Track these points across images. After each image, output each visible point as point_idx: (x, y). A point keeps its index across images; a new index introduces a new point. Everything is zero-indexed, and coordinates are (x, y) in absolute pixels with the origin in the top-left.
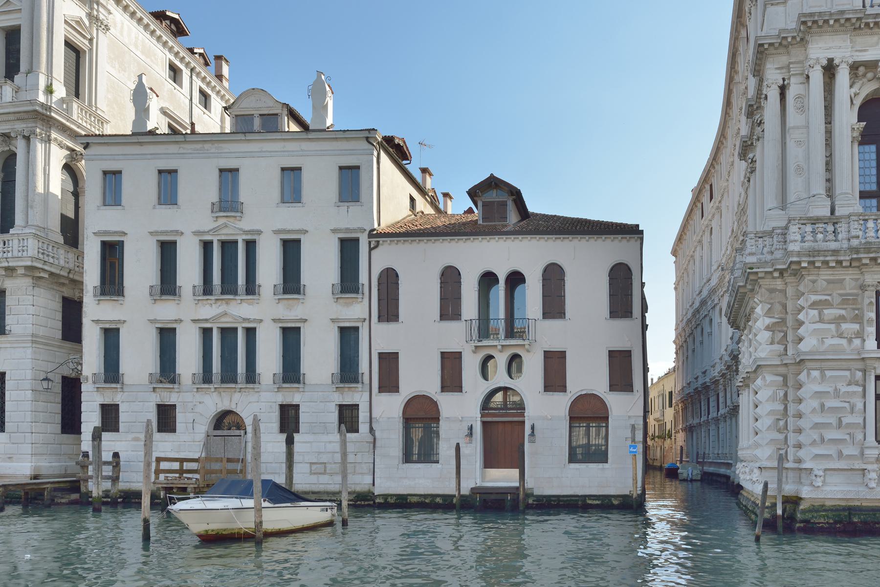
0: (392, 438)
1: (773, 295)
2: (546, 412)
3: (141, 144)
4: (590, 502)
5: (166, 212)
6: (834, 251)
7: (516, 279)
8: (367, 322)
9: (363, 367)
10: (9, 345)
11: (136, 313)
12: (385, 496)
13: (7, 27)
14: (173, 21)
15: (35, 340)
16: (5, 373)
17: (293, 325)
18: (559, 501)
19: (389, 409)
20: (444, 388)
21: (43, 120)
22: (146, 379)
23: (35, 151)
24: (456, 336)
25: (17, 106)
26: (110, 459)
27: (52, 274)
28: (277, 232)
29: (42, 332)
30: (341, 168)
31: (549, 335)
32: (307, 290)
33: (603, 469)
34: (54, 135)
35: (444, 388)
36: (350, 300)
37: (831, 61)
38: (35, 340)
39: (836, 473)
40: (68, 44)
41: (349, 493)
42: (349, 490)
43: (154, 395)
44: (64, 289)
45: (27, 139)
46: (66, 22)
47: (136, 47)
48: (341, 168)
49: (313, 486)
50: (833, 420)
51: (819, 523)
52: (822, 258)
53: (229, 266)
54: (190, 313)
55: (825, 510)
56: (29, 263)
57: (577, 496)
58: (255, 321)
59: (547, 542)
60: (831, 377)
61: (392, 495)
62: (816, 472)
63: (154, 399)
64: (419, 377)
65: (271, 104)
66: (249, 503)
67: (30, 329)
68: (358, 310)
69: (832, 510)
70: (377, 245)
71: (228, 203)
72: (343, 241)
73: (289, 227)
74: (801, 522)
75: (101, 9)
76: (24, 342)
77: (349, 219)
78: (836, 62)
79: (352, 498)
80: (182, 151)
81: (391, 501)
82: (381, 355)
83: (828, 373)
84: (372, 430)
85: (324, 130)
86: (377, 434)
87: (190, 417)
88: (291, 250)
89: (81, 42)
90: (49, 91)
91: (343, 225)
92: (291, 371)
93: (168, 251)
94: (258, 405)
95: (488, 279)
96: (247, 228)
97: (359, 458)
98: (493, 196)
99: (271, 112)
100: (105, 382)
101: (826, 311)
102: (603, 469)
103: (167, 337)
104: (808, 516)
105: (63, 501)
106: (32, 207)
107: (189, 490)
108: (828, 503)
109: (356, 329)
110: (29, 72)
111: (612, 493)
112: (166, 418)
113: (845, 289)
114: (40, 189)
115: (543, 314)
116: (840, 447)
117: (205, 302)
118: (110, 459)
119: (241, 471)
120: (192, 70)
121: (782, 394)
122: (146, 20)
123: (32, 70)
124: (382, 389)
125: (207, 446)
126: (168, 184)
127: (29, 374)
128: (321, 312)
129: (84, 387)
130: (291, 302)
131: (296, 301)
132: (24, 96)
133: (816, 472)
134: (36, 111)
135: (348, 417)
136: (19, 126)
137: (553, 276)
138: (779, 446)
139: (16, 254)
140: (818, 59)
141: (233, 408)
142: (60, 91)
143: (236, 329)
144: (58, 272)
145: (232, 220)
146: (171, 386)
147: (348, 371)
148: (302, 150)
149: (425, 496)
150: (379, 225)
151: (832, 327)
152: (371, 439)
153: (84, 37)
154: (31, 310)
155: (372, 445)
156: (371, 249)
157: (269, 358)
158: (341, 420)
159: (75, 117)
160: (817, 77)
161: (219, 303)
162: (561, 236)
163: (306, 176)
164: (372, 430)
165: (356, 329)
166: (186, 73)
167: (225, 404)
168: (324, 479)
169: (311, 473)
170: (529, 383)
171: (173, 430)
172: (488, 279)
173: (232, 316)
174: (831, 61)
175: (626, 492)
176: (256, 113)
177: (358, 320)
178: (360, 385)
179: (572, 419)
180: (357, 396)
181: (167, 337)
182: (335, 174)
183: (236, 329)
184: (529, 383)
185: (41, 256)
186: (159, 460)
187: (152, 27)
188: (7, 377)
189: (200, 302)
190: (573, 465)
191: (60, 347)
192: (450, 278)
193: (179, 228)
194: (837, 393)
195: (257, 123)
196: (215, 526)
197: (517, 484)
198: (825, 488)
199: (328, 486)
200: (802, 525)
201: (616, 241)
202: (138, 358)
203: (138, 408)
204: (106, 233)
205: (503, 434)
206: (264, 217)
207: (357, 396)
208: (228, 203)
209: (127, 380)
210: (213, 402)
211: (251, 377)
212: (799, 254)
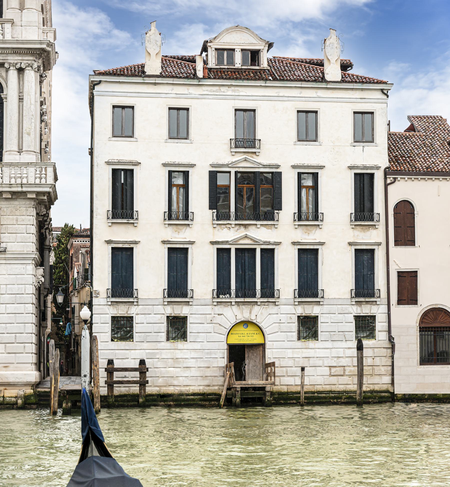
9: (380, 282)
22: (160, 295)
45: (21, 71)
49: (333, 386)
73: (306, 163)
82: (400, 274)
84: (391, 339)
91: (359, 163)
92: (308, 286)
97: (377, 361)
112: (177, 327)
124: (400, 302)
135: (365, 325)
139: (31, 181)
143: (255, 250)
144: (19, 189)
147: (364, 287)
158: (358, 328)
164: (391, 339)
165: (372, 252)
169: (331, 375)
179: (422, 329)
181: (178, 258)
199: (348, 386)
202: (150, 275)
208: (246, 140)
211: (269, 291)
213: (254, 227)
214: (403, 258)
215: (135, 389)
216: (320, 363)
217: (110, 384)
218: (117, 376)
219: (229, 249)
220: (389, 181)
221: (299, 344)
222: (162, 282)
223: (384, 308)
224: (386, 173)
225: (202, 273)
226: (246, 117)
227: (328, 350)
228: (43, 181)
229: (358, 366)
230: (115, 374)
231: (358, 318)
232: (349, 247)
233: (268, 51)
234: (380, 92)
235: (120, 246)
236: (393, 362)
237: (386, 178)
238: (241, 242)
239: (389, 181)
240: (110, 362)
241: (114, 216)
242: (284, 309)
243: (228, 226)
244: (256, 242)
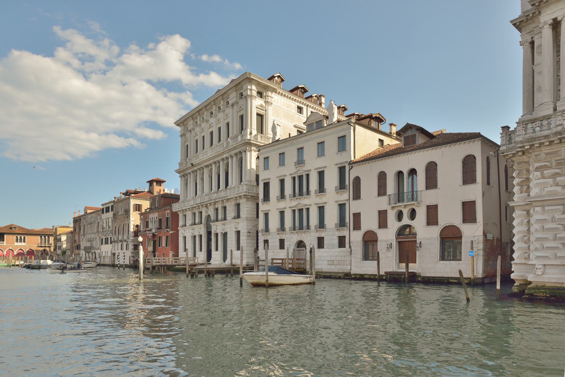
0: (358, 249)
1: (521, 165)
2: (427, 236)
3: (274, 146)
4: (451, 281)
5: (282, 168)
6: (545, 136)
7: (413, 172)
11: (273, 207)
12: (355, 275)
14: (303, 88)
15: (247, 219)
19: (356, 237)
27: (252, 196)
28: (316, 169)
29: (249, 216)
31: (429, 197)
35: (464, 221)
37: (555, 20)
38: (247, 219)
39: (553, 267)
40: (258, 114)
46: (257, 108)
47: (283, 106)
50: (550, 235)
51: (539, 296)
52: (538, 142)
53: (301, 185)
54: (289, 204)
55: (544, 289)
59: (427, 300)
60: (548, 210)
61: (358, 274)
62: (537, 266)
63: (278, 237)
64: (369, 223)
66: (264, 273)
69: (549, 289)
70: (352, 167)
71: (300, 162)
74: (527, 294)
77: (342, 159)
78: (559, 19)
81: (358, 277)
82: (354, 214)
83: (546, 208)
84: (350, 247)
86: (352, 248)
88: (321, 174)
89: (262, 112)
90: (251, 133)
92: (322, 225)
94: (310, 239)
95: (400, 174)
98: (409, 133)
101: (545, 172)
102: (459, 264)
104: (532, 291)
108: (548, 285)
113: (561, 156)
114: (249, 168)
116: (556, 251)
119: (304, 264)
120: (307, 106)
121: (526, 221)
122: (287, 95)
123: (246, 129)
124: (354, 229)
128: (332, 198)
133: (537, 266)
135: (342, 242)
136: (243, 148)
138: (525, 251)
140: (545, 22)
142: (254, 132)
147: (342, 223)
149: (371, 275)
150: (355, 158)
151: (550, 181)
157: (314, 220)
159: (259, 140)
160: (547, 32)
164: (350, 247)
166: (305, 108)
167: (299, 239)
168: (333, 267)
170: (419, 224)
171: (323, 248)
172: (400, 174)
174: (555, 20)
176: (314, 122)
177: (345, 200)
180: (344, 232)
186: (272, 259)
187: (289, 96)
190: (442, 262)
192: (382, 177)
193: (309, 168)
194: (553, 220)
196: (256, 281)
197: (404, 271)
198: (543, 276)
200: (527, 296)
201: (466, 144)
202: (274, 223)
205: (407, 247)
206: (312, 164)
207: (344, 232)
208: (300, 162)
211: (308, 227)
212: (521, 142)
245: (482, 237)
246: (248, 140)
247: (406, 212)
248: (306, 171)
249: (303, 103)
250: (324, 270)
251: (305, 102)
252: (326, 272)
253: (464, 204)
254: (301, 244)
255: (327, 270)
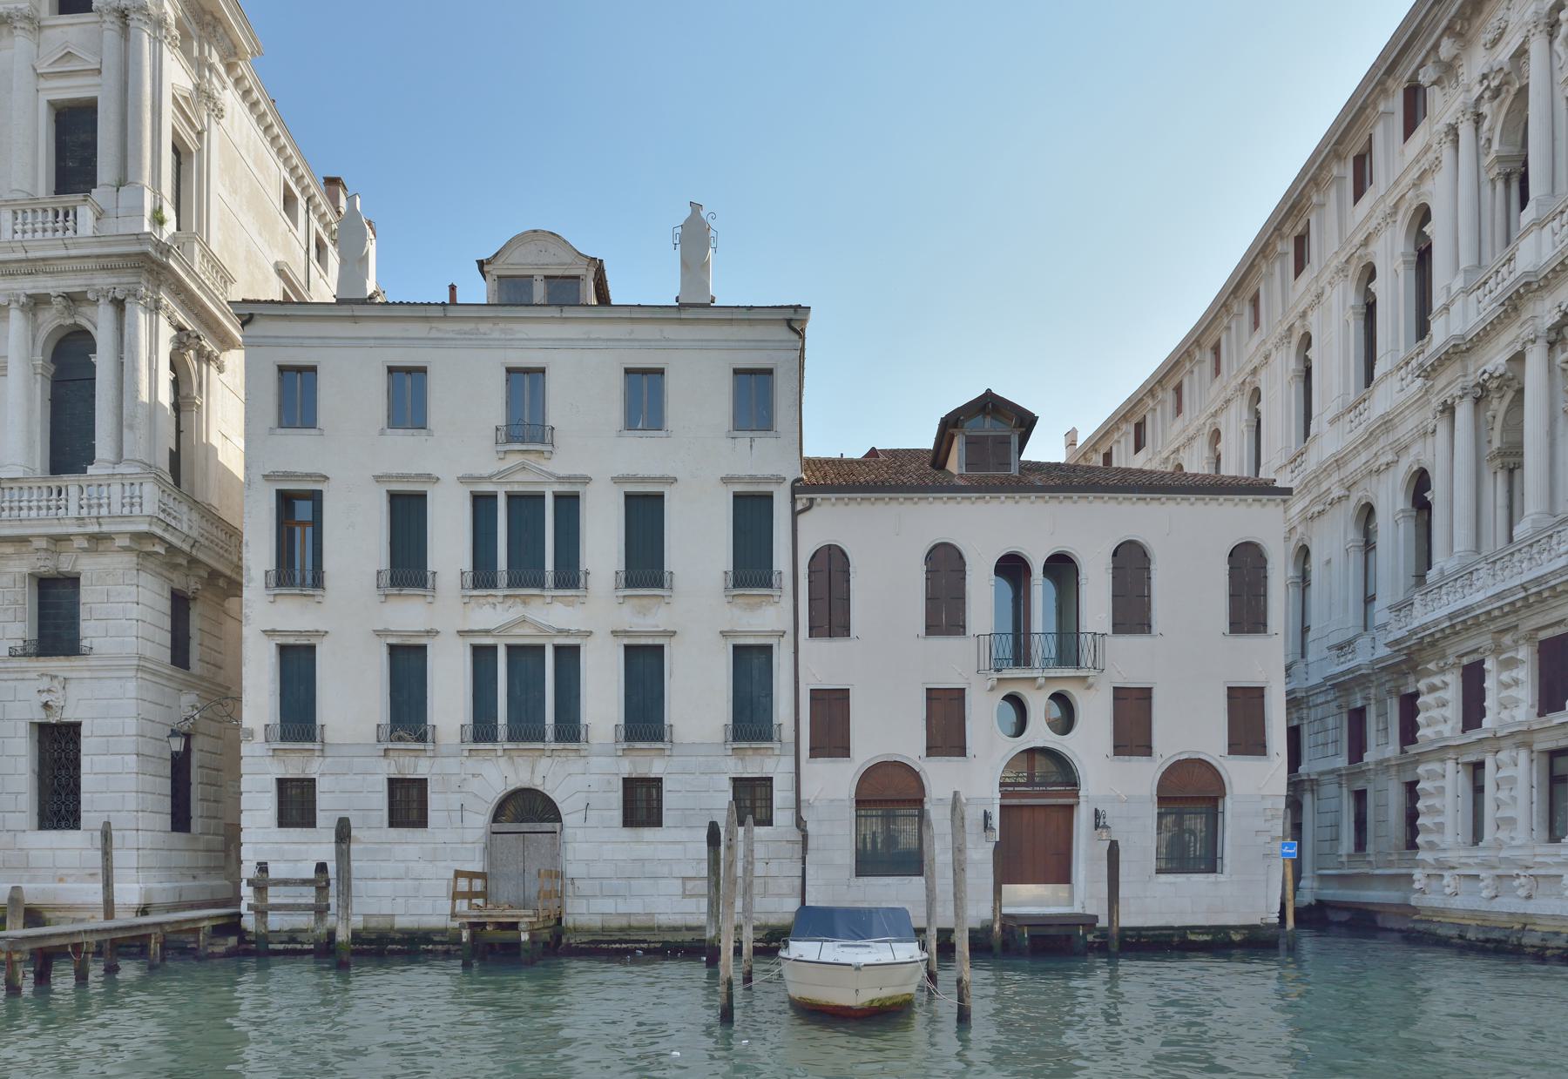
0: (837, 835)
3: (355, 319)
4: (1193, 937)
5: (404, 440)
8: (789, 638)
9: (782, 711)
10: (87, 674)
13: (63, 101)
16: (79, 724)
17: (650, 641)
18: (1140, 936)
19: (831, 784)
20: (932, 750)
21: (150, 272)
22: (720, 738)
23: (136, 326)
24: (956, 662)
25: (109, 244)
26: (311, 875)
27: (171, 548)
28: (617, 480)
30: (736, 372)
31: (1127, 659)
32: (677, 582)
33: (1216, 883)
34: (165, 300)
35: (932, 750)
36: (757, 600)
41: (755, 928)
42: (756, 923)
43: (384, 762)
44: (174, 576)
45: (119, 305)
48: (736, 372)
53: (526, 538)
54: (456, 618)
56: (144, 528)
57: (1172, 928)
58: (579, 633)
64: (887, 730)
65: (567, 258)
67: (131, 645)
68: (771, 617)
72: (394, 497)
75: (215, 80)
76: (120, 668)
77: (765, 462)
79: (760, 936)
80: (434, 334)
84: (800, 823)
85: (707, 306)
86: (810, 828)
87: (455, 800)
88: (645, 514)
90: (159, 220)
92: (645, 716)
93: (407, 512)
96: (562, 473)
97: (774, 869)
99: (567, 273)
100: (282, 739)
102: (1216, 883)
103: (407, 665)
105: (218, 949)
106: (131, 427)
107: (522, 926)
109: (768, 649)
110: (122, 182)
111: (1232, 923)
112: (408, 804)
114: (144, 397)
115: (927, 627)
117: (482, 600)
118: (311, 875)
124: (816, 752)
125: (489, 851)
126: (407, 396)
127: (132, 727)
128: (700, 619)
129: (245, 749)
130: (645, 601)
131: (655, 600)
132: (112, 227)
134: (146, 254)
136: (103, 281)
137: (1131, 564)
139: (116, 509)
141: (537, 784)
145: (532, 457)
146: (420, 746)
147: (750, 718)
148: (668, 340)
152: (797, 836)
153: (192, 125)
154: (135, 611)
155: (799, 847)
156: (795, 514)
157: (603, 697)
161: (510, 602)
162: (1149, 496)
163: (672, 383)
164: (800, 823)
165: (768, 649)
169: (684, 895)
170: (1089, 744)
171: (422, 822)
172: (1012, 568)
173: (535, 625)
175: (1255, 920)
176: (539, 273)
177: (772, 634)
178: (776, 745)
179: (860, 803)
180: (773, 765)
181: (407, 665)
182: (726, 384)
183: (542, 648)
184: (1089, 744)
185: (162, 516)
188: (84, 731)
189: (473, 601)
191: (170, 678)
192: (945, 566)
195: (539, 292)
202: (352, 697)
203: (352, 783)
204: (288, 476)
205: (1036, 827)
206: (592, 452)
207: (773, 765)
208: (526, 421)
209: (330, 736)
210: (501, 772)
211: (570, 729)
213: (539, 601)
214: (823, 663)
215: (304, 921)
216: (665, 870)
217: (261, 912)
218: (275, 896)
219: (494, 648)
220: (799, 507)
221: (628, 833)
222: (721, 710)
223: (788, 763)
224: (797, 488)
225: (449, 695)
226: (525, 383)
227: (680, 847)
228: (136, 510)
229: (709, 878)
230: (271, 890)
231: (738, 783)
232: (460, 640)
233: (1297, 274)
234: (785, 328)
235: (643, 641)
236: (804, 870)
237: (794, 501)
238: (517, 631)
239: (799, 507)
240: (263, 868)
241: (738, 583)
242: (599, 764)
243: (490, 600)
244: (543, 630)
245: (725, 813)
246: (158, 244)
247: (1039, 705)
248: (561, 480)
249: (304, 190)
250: (663, 920)
251: (313, 190)
252: (675, 929)
253: (1233, 692)
254: (527, 809)
255: (678, 920)
